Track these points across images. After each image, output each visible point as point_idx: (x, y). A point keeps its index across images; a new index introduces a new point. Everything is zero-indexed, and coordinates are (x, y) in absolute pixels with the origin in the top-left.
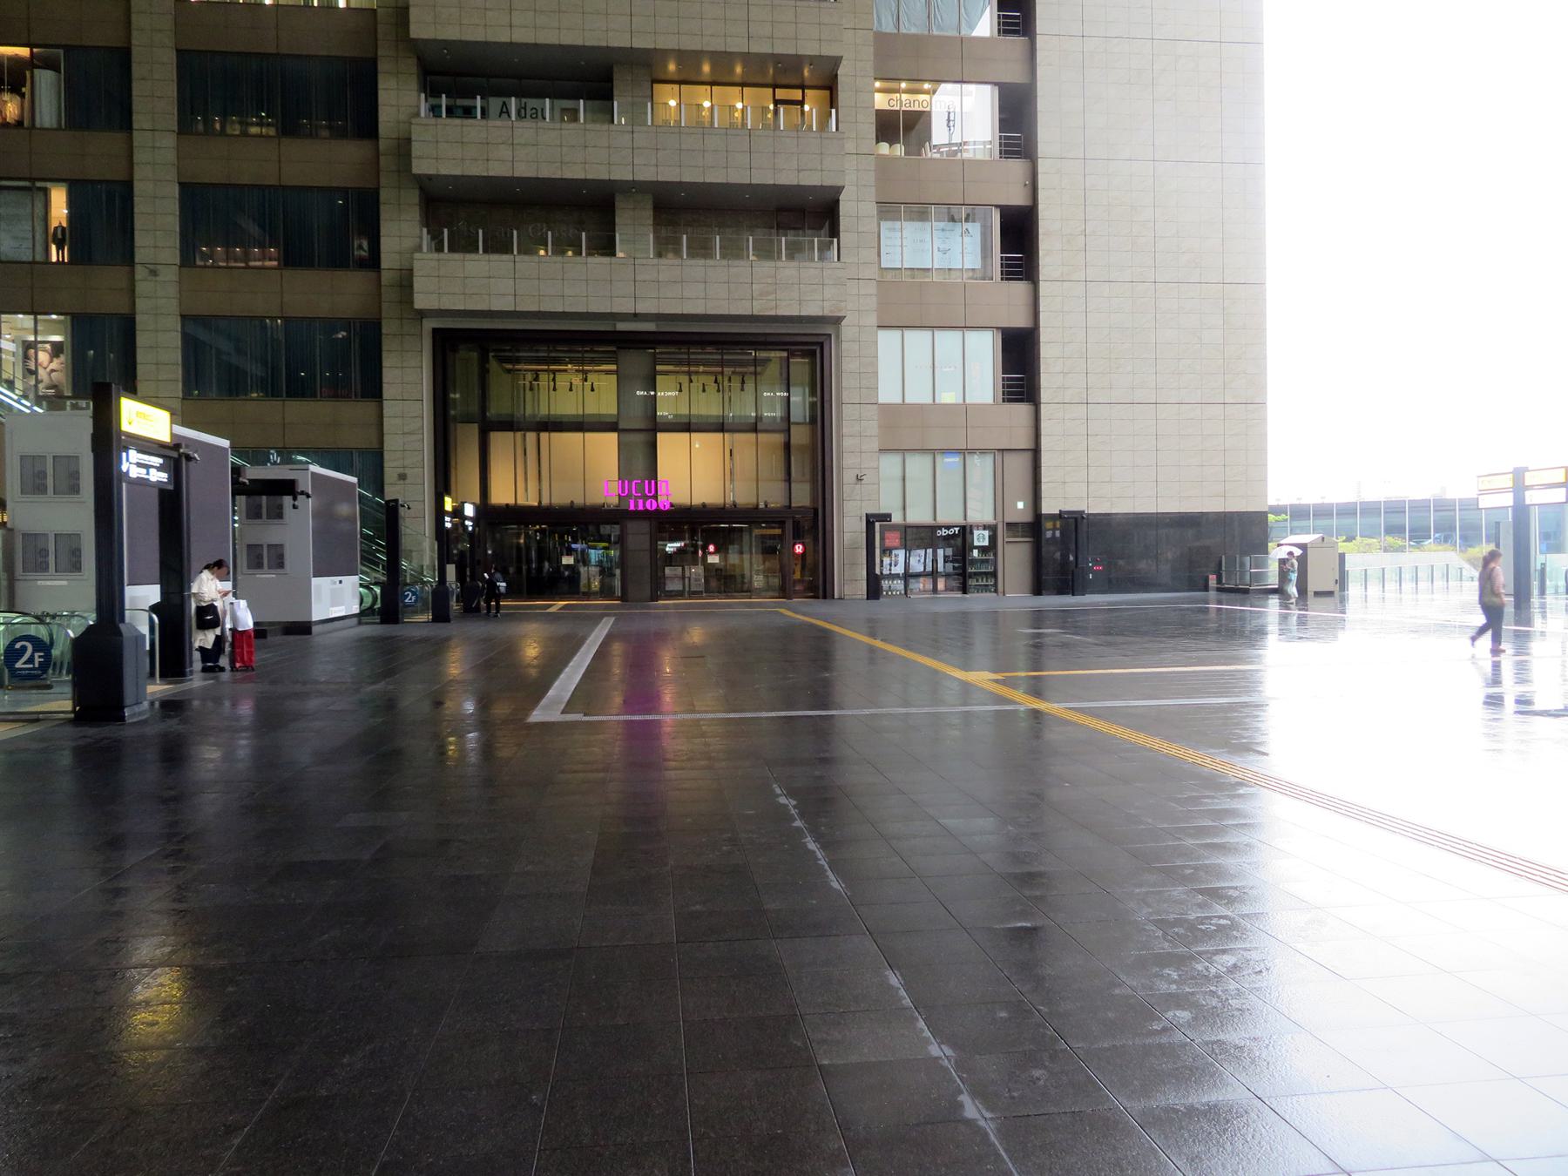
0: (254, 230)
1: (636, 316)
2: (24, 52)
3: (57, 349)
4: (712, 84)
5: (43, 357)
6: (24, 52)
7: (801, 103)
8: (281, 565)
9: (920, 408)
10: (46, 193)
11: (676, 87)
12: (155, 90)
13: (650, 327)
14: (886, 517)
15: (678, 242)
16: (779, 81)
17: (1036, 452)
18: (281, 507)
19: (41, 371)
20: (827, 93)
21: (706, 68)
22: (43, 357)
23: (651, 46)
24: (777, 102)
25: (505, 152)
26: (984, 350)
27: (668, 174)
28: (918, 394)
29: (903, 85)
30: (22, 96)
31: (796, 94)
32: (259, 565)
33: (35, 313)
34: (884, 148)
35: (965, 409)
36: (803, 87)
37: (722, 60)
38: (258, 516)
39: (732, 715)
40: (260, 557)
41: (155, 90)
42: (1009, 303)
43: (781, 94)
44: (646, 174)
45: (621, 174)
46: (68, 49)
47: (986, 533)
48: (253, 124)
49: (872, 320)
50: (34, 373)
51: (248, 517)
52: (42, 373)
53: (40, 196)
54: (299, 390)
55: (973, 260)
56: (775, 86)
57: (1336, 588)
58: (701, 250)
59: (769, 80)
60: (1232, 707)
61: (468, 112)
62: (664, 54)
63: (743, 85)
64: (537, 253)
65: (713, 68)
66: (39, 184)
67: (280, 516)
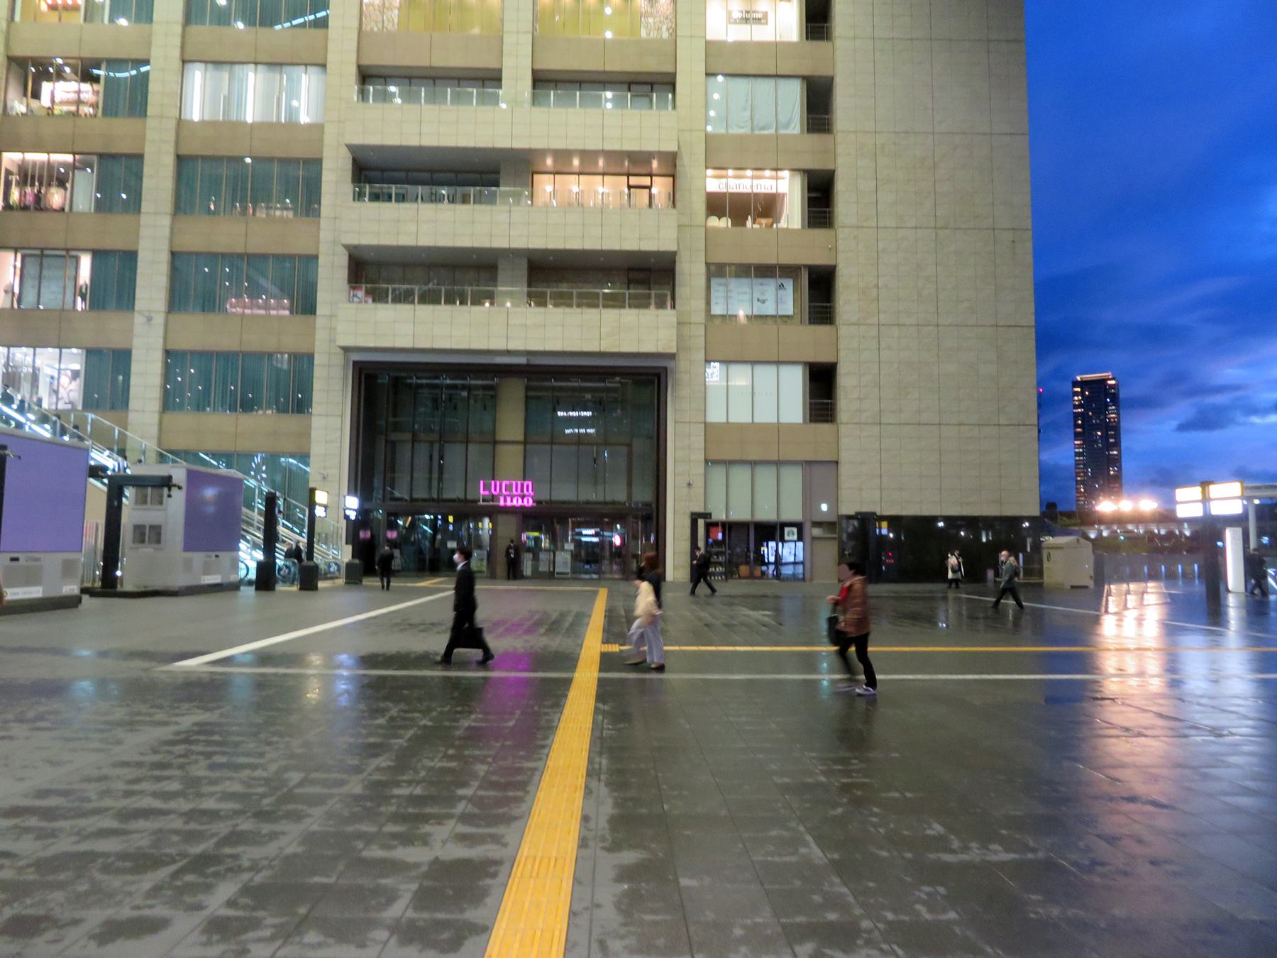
0: (275, 290)
1: (509, 353)
2: (69, 158)
3: (75, 374)
4: (579, 174)
5: (65, 380)
6: (69, 158)
7: (649, 188)
8: (158, 541)
9: (741, 427)
10: (77, 259)
11: (552, 176)
12: (158, 180)
13: (523, 360)
14: (706, 515)
15: (649, 297)
16: (632, 171)
17: (809, 463)
18: (161, 496)
19: (61, 390)
20: (671, 179)
21: (576, 162)
22: (65, 380)
23: (527, 146)
24: (630, 187)
25: (412, 228)
26: (794, 381)
27: (537, 243)
28: (740, 415)
29: (730, 172)
30: (66, 189)
31: (646, 181)
32: (143, 541)
33: (60, 348)
34: (714, 222)
35: (779, 428)
36: (651, 175)
37: (588, 156)
38: (145, 502)
39: (282, 671)
40: (143, 534)
41: (158, 180)
42: (814, 342)
43: (634, 180)
44: (519, 243)
45: (501, 243)
46: (101, 156)
47: (795, 530)
48: (276, 209)
49: (701, 356)
50: (56, 392)
51: (137, 502)
52: (62, 393)
53: (71, 263)
54: (248, 406)
55: (788, 308)
56: (628, 175)
57: (1091, 584)
58: (563, 300)
59: (625, 170)
60: (1084, 682)
61: (465, 200)
62: (542, 153)
63: (604, 174)
64: (483, 304)
65: (555, 161)
66: (73, 253)
67: (161, 503)
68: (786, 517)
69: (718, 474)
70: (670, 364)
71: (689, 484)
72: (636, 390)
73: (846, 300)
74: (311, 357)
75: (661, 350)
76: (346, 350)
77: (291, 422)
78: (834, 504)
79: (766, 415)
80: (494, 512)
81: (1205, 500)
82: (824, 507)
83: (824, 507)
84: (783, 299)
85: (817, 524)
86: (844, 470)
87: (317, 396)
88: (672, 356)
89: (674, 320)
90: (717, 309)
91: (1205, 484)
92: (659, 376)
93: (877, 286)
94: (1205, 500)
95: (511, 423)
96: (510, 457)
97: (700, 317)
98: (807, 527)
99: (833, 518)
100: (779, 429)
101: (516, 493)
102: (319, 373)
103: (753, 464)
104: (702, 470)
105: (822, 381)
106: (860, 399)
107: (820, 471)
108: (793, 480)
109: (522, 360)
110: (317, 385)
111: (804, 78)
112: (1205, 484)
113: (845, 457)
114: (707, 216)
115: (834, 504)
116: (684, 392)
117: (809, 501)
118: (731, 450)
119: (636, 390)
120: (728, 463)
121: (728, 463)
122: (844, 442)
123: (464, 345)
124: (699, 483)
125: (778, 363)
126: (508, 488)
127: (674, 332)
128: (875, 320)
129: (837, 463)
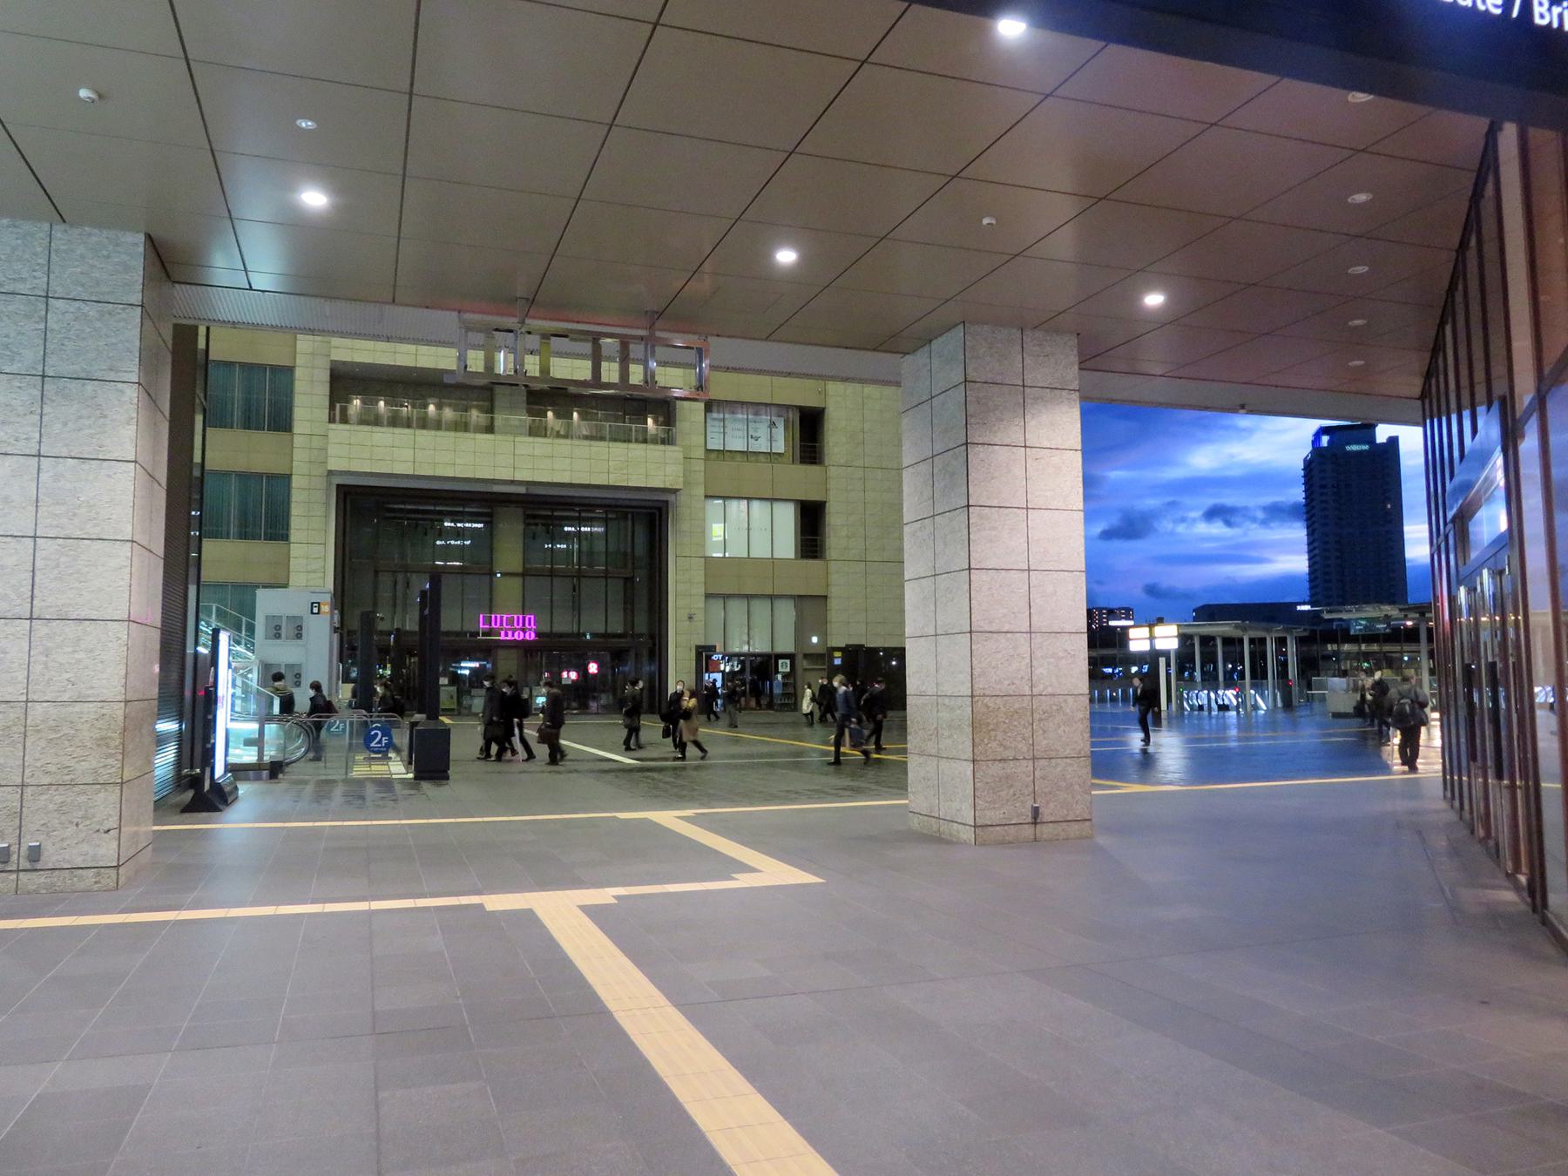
26: (787, 517)
40: (278, 628)
42: (805, 481)
49: (701, 491)
55: (780, 446)
68: (780, 649)
69: (717, 605)
70: (671, 498)
71: (690, 618)
72: (647, 518)
73: (835, 440)
74: (287, 478)
75: (668, 486)
76: (331, 473)
77: (262, 550)
78: (824, 636)
79: (761, 550)
80: (486, 649)
81: (1152, 638)
82: (815, 640)
83: (815, 640)
84: (774, 438)
85: (806, 656)
86: (833, 604)
87: (295, 522)
88: (675, 491)
89: (681, 456)
90: (714, 444)
91: (1151, 626)
92: (660, 509)
93: (863, 431)
94: (1152, 638)
95: (509, 554)
96: (508, 590)
97: (700, 453)
98: (799, 658)
99: (821, 651)
100: (773, 563)
101: (514, 625)
102: (297, 497)
103: (749, 597)
104: (702, 605)
105: (811, 518)
106: (848, 537)
107: (812, 605)
108: (786, 614)
109: (522, 490)
110: (295, 510)
111: (796, 501)
112: (1151, 626)
113: (835, 592)
114: (796, 501)
115: (824, 636)
116: (685, 526)
117: (800, 634)
118: (732, 585)
119: (647, 518)
120: (726, 597)
121: (726, 597)
122: (834, 578)
123: (566, 479)
124: (700, 616)
125: (772, 500)
126: (510, 622)
127: (681, 468)
128: (860, 463)
129: (826, 597)
